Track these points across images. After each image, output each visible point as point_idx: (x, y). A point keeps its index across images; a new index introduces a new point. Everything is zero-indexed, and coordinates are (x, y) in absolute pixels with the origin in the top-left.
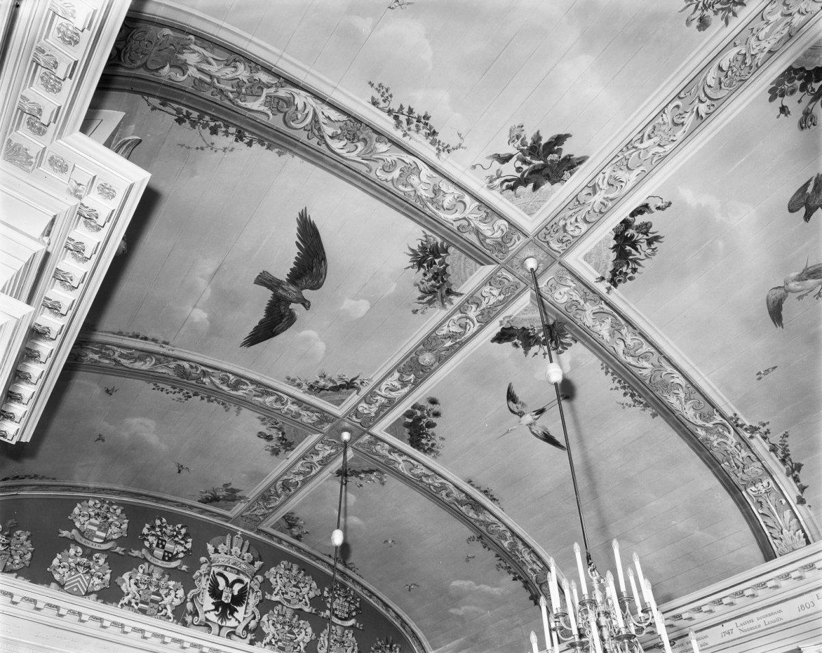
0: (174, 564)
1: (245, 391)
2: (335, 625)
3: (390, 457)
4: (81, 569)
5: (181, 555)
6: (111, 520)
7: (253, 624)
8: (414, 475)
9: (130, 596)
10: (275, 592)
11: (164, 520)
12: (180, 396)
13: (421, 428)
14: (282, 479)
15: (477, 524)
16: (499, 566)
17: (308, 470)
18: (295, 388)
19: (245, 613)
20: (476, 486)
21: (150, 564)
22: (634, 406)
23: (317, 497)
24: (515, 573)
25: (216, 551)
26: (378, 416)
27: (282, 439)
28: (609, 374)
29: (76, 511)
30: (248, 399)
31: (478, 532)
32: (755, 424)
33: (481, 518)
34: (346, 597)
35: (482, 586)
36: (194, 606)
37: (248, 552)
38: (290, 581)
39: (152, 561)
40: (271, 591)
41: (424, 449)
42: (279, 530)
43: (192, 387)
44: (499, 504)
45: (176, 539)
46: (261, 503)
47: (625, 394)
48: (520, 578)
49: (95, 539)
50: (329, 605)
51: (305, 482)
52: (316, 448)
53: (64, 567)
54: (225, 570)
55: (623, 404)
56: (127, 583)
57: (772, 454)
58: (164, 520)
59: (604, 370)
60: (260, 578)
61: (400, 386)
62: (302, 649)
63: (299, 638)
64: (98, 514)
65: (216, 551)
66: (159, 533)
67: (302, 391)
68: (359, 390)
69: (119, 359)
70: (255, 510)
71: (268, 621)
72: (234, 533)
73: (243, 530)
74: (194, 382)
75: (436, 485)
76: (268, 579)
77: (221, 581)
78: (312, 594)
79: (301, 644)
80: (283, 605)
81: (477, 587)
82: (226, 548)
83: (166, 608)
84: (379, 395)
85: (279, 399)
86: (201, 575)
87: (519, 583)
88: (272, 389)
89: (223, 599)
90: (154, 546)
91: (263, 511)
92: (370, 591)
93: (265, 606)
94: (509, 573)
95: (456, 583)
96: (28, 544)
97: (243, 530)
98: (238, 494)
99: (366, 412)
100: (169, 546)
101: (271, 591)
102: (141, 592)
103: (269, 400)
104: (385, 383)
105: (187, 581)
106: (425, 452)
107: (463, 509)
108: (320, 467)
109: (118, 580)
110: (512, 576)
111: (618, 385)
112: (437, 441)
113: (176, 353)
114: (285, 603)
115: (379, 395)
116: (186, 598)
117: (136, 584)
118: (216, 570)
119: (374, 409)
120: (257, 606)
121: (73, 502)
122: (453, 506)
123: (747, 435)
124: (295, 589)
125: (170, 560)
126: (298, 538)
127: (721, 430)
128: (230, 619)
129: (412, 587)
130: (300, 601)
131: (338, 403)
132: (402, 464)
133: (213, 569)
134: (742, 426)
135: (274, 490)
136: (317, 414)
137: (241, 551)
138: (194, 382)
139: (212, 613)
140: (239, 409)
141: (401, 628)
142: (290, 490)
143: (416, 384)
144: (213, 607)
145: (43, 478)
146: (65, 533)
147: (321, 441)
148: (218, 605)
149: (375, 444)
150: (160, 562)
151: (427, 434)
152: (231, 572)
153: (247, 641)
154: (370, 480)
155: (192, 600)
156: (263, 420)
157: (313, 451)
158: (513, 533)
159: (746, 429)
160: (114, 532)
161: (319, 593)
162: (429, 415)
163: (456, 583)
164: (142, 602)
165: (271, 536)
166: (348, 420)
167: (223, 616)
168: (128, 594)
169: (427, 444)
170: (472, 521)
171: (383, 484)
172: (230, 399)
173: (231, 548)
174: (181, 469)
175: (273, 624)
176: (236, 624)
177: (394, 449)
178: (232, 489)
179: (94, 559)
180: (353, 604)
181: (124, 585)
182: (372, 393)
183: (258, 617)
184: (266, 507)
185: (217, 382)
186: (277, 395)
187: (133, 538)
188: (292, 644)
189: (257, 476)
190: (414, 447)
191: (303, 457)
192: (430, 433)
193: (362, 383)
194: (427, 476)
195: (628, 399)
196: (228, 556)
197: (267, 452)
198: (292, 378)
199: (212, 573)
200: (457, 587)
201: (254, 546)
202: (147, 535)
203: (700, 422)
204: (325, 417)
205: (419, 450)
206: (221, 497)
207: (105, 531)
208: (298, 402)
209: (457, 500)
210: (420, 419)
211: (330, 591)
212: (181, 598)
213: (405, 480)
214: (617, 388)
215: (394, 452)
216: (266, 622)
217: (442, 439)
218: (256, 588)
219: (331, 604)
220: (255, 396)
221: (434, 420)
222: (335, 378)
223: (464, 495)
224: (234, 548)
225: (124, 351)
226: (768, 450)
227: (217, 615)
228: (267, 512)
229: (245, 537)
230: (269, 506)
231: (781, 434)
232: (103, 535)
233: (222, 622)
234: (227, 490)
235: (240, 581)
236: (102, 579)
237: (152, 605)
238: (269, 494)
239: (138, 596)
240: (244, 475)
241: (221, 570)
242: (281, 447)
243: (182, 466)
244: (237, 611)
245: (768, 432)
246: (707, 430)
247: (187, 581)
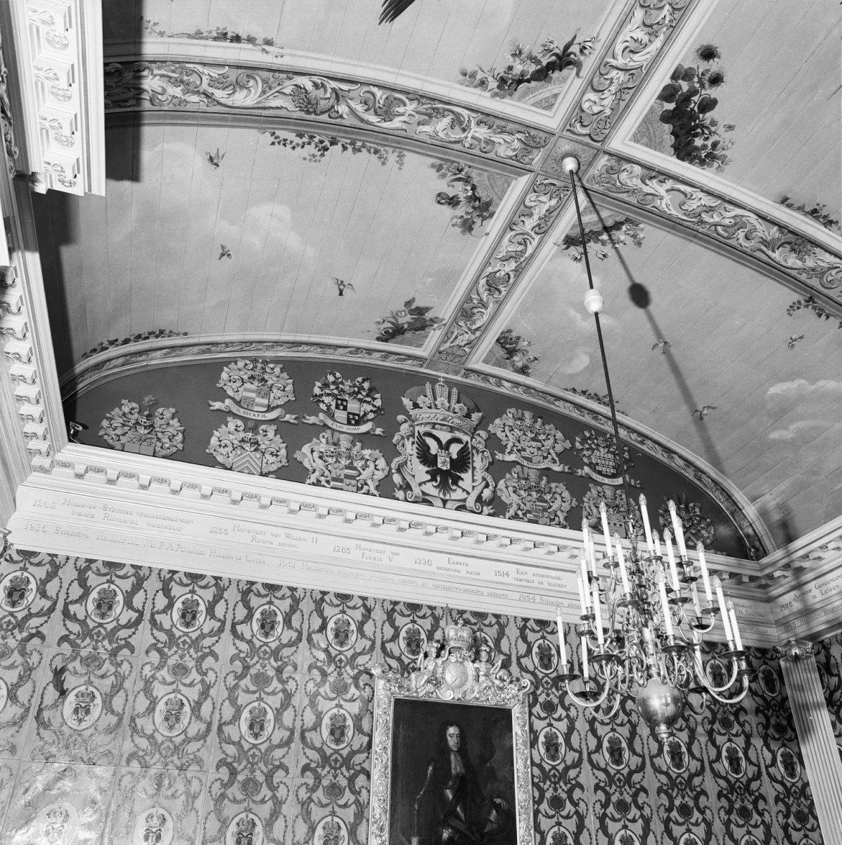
0: (364, 428)
1: (404, 118)
2: (602, 484)
3: (646, 189)
4: (247, 446)
5: (371, 416)
6: (270, 382)
7: (487, 494)
9: (317, 473)
10: (508, 450)
11: (338, 375)
12: (311, 149)
13: (693, 116)
14: (484, 274)
15: (803, 277)
18: (478, 91)
19: (473, 481)
20: (796, 206)
21: (333, 430)
23: (541, 296)
25: (416, 406)
26: (619, 112)
27: (474, 198)
29: (224, 376)
30: (410, 134)
31: (805, 291)
33: (810, 263)
35: (821, 383)
37: (458, 402)
38: (525, 434)
39: (334, 427)
40: (502, 449)
41: (700, 158)
42: (495, 365)
43: (325, 129)
45: (360, 396)
46: (461, 323)
49: (256, 409)
50: (586, 460)
51: (519, 272)
52: (528, 203)
53: (226, 446)
54: (434, 428)
56: (308, 455)
58: (338, 375)
60: (483, 434)
61: (646, 39)
62: (562, 520)
63: (555, 506)
64: (252, 377)
65: (416, 406)
66: (336, 392)
67: (488, 94)
68: (578, 65)
69: (211, 90)
70: (456, 337)
71: (507, 487)
72: (434, 381)
73: (446, 375)
74: (325, 117)
75: (727, 222)
76: (495, 434)
77: (433, 447)
78: (559, 448)
79: (559, 513)
80: (522, 466)
81: (813, 387)
82: (429, 401)
83: (366, 484)
85: (457, 121)
86: (403, 438)
88: (441, 102)
89: (439, 465)
90: (333, 407)
91: (467, 336)
92: (640, 434)
93: (497, 469)
95: (776, 389)
96: (175, 422)
97: (446, 375)
98: (428, 316)
99: (596, 109)
100: (353, 406)
101: (502, 449)
102: (330, 467)
103: (442, 125)
104: (620, 39)
105: (390, 452)
106: (702, 163)
107: (777, 255)
108: (537, 238)
109: (297, 455)
112: (722, 135)
113: (288, 62)
114: (525, 463)
116: (390, 469)
117: (321, 458)
118: (422, 429)
119: (609, 99)
120: (487, 470)
121: (219, 365)
122: (758, 254)
124: (534, 444)
125: (358, 423)
126: (523, 370)
128: (455, 490)
129: (705, 412)
130: (545, 458)
131: (548, 105)
132: (667, 198)
133: (417, 428)
135: (476, 297)
136: (519, 136)
137: (449, 402)
138: (325, 117)
139: (429, 484)
140: (401, 156)
141: (698, 482)
142: (500, 292)
143: (674, 27)
144: (429, 477)
145: (171, 334)
146: (217, 405)
147: (533, 188)
148: (434, 473)
149: (619, 172)
150: (345, 427)
151: (703, 127)
152: (441, 430)
155: (399, 471)
156: (439, 168)
157: (523, 210)
160: (278, 397)
161: (568, 445)
162: (702, 86)
163: (776, 389)
164: (334, 479)
165: (485, 376)
166: (569, 134)
167: (444, 487)
168: (314, 471)
169: (704, 147)
170: (794, 273)
171: (639, 244)
172: (386, 140)
173: (435, 399)
174: (342, 287)
175: (515, 492)
176: (464, 495)
178: (418, 308)
179: (261, 432)
181: (306, 460)
182: (603, 67)
183: (492, 483)
184: (470, 330)
185: (360, 108)
186: (453, 112)
187: (303, 402)
188: (546, 514)
189: (447, 278)
190: (683, 159)
191: (510, 226)
192: (707, 122)
193: (582, 49)
194: (711, 209)
196: (434, 410)
197: (456, 228)
198: (469, 71)
199: (416, 434)
200: (778, 395)
201: (465, 392)
202: (321, 395)
204: (533, 138)
205: (691, 162)
206: (406, 326)
207: (267, 395)
208: (486, 118)
209: (764, 242)
210: (687, 98)
211: (584, 440)
212: (383, 470)
213: (673, 228)
215: (651, 178)
216: (505, 490)
217: (730, 128)
218: (481, 447)
219: (589, 457)
220: (419, 124)
221: (713, 92)
222: (537, 52)
223: (776, 228)
224: (439, 399)
225: (215, 73)
227: (435, 487)
228: (473, 337)
229: (449, 383)
230: (474, 327)
232: (265, 402)
233: (444, 494)
234: (411, 312)
236: (277, 456)
237: (348, 481)
238: (472, 305)
239: (327, 473)
240: (430, 280)
241: (428, 429)
242: (475, 214)
243: (342, 282)
247: (390, 452)
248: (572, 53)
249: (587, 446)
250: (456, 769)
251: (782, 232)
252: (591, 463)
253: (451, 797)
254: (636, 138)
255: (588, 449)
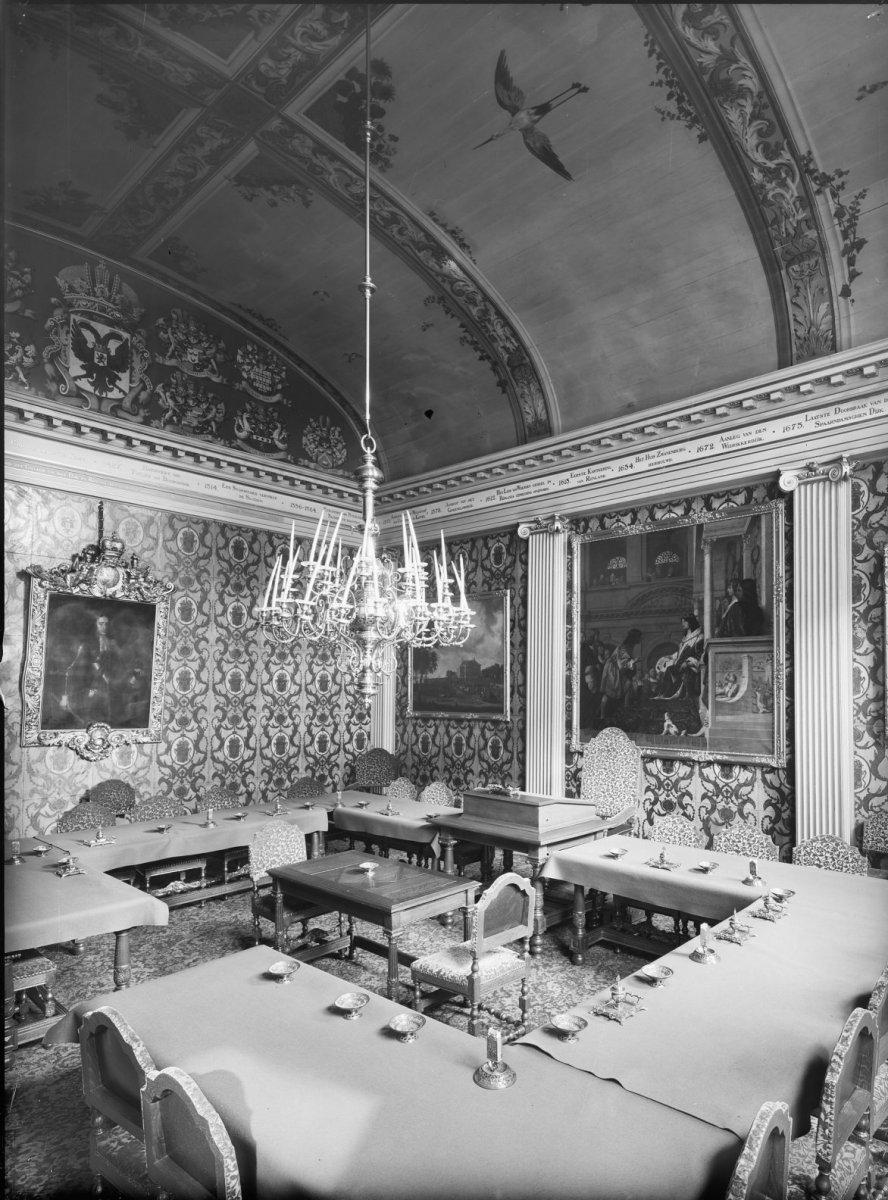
2: (256, 400)
7: (143, 396)
8: (352, 195)
16: (463, 340)
17: (189, 170)
22: (679, 118)
24: (483, 351)
28: (654, 56)
32: (830, 173)
34: (268, 364)
36: (57, 371)
44: (470, 252)
47: (670, 96)
48: (488, 358)
50: (245, 375)
55: (663, 113)
57: (836, 221)
59: (647, 48)
61: (325, 33)
75: (385, 214)
79: (213, 423)
84: (293, 46)
86: (56, 325)
87: (487, 364)
94: (476, 349)
99: (272, 75)
110: (479, 354)
111: (663, 78)
115: (293, 46)
118: (78, 318)
122: (406, 248)
123: (814, 187)
127: (783, 175)
133: (73, 316)
134: (811, 172)
137: (110, 291)
148: (90, 369)
153: (139, 419)
154: (288, 196)
155: (51, 361)
158: (486, 298)
159: (816, 179)
170: (433, 274)
176: (121, 396)
177: (321, 149)
180: (278, 374)
183: (150, 387)
195: (672, 106)
199: (72, 323)
203: (759, 157)
214: (660, 83)
217: (394, 139)
218: (141, 347)
219: (248, 372)
223: (422, 234)
226: (833, 212)
231: (856, 193)
233: (101, 393)
235: (118, 337)
244: (120, 380)
245: (842, 187)
246: (764, 170)
248: (250, 16)
249: (248, 361)
250: (103, 648)
251: (427, 239)
252: (249, 378)
253: (98, 668)
254: (309, 114)
255: (248, 364)
